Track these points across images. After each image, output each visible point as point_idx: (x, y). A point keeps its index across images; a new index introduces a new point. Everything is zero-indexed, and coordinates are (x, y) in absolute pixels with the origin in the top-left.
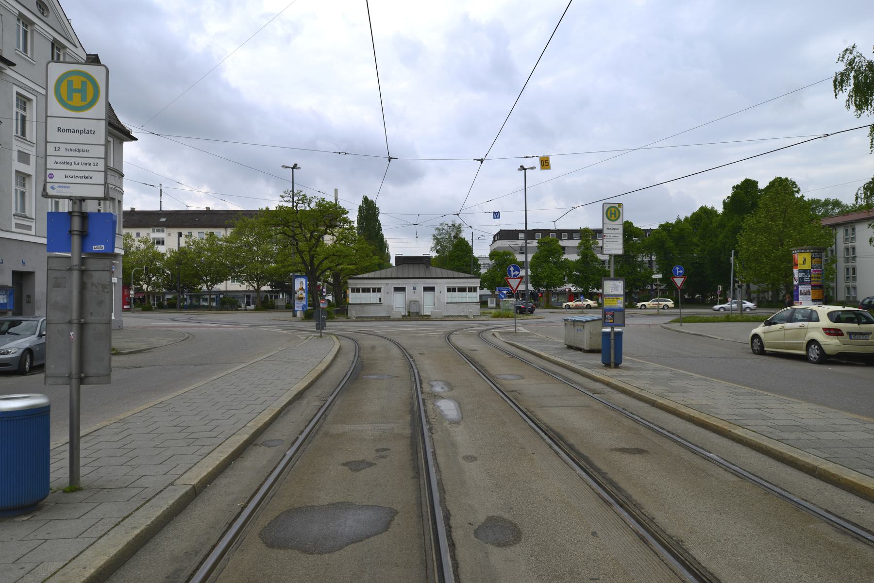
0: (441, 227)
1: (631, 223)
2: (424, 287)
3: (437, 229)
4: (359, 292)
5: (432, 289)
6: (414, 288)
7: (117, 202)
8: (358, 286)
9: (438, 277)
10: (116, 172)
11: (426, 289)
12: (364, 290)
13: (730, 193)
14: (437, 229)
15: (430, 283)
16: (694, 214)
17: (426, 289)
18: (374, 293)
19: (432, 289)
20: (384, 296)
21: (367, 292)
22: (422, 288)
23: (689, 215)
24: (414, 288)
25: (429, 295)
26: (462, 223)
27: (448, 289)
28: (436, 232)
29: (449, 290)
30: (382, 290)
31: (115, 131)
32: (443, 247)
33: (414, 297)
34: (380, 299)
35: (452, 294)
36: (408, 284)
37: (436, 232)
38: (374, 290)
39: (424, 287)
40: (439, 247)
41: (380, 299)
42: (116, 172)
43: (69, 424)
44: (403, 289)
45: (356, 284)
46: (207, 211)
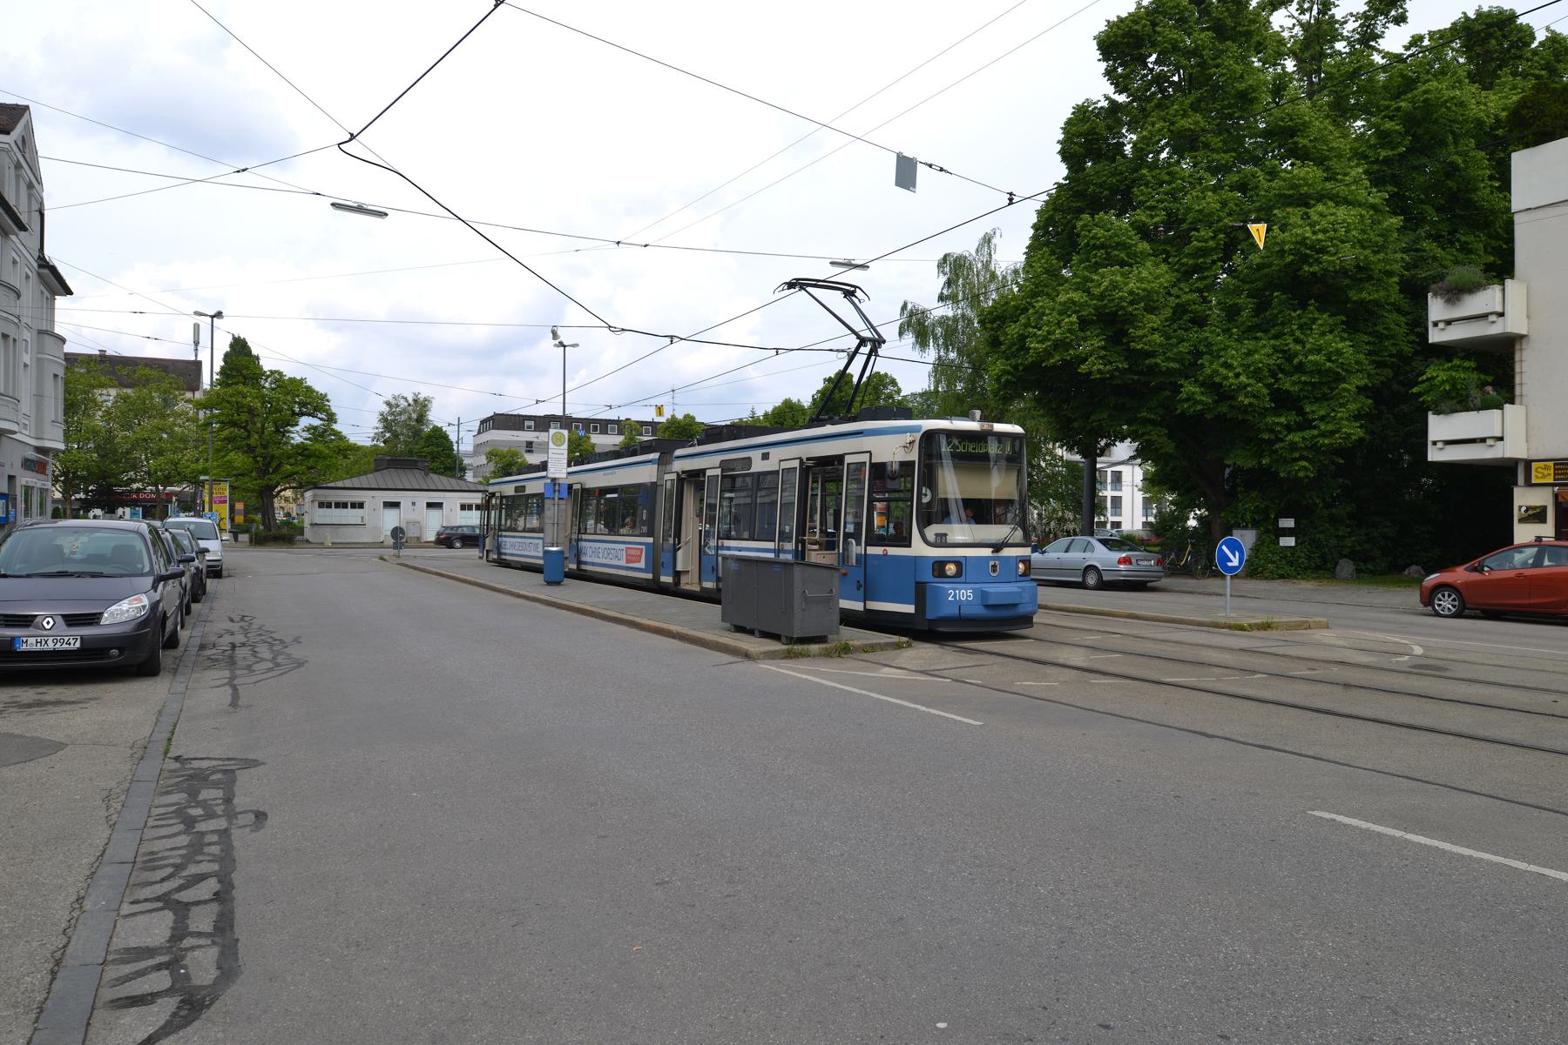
0: (393, 402)
1: (693, 418)
2: (427, 503)
3: (388, 404)
4: (347, 507)
5: (439, 505)
6: (414, 504)
7: (11, 340)
8: (329, 499)
9: (381, 487)
10: (13, 290)
11: (430, 505)
12: (338, 505)
13: (820, 386)
14: (388, 404)
15: (435, 497)
16: (775, 408)
17: (430, 505)
18: (337, 510)
19: (439, 505)
20: (369, 514)
21: (359, 508)
22: (425, 504)
23: (770, 409)
24: (414, 504)
25: (434, 513)
26: (1136, 489)
27: (461, 506)
28: (386, 409)
29: (463, 507)
30: (366, 505)
31: (7, 218)
32: (396, 435)
33: (413, 516)
34: (362, 518)
35: (466, 513)
36: (404, 498)
37: (386, 409)
38: (354, 506)
39: (427, 503)
40: (388, 435)
41: (362, 518)
42: (13, 290)
43: (1507, 455)
44: (396, 505)
45: (326, 496)
46: (100, 356)
